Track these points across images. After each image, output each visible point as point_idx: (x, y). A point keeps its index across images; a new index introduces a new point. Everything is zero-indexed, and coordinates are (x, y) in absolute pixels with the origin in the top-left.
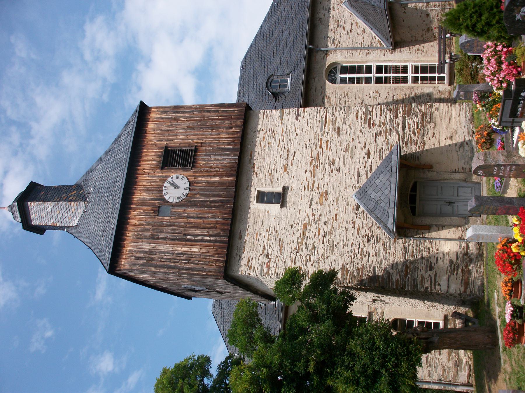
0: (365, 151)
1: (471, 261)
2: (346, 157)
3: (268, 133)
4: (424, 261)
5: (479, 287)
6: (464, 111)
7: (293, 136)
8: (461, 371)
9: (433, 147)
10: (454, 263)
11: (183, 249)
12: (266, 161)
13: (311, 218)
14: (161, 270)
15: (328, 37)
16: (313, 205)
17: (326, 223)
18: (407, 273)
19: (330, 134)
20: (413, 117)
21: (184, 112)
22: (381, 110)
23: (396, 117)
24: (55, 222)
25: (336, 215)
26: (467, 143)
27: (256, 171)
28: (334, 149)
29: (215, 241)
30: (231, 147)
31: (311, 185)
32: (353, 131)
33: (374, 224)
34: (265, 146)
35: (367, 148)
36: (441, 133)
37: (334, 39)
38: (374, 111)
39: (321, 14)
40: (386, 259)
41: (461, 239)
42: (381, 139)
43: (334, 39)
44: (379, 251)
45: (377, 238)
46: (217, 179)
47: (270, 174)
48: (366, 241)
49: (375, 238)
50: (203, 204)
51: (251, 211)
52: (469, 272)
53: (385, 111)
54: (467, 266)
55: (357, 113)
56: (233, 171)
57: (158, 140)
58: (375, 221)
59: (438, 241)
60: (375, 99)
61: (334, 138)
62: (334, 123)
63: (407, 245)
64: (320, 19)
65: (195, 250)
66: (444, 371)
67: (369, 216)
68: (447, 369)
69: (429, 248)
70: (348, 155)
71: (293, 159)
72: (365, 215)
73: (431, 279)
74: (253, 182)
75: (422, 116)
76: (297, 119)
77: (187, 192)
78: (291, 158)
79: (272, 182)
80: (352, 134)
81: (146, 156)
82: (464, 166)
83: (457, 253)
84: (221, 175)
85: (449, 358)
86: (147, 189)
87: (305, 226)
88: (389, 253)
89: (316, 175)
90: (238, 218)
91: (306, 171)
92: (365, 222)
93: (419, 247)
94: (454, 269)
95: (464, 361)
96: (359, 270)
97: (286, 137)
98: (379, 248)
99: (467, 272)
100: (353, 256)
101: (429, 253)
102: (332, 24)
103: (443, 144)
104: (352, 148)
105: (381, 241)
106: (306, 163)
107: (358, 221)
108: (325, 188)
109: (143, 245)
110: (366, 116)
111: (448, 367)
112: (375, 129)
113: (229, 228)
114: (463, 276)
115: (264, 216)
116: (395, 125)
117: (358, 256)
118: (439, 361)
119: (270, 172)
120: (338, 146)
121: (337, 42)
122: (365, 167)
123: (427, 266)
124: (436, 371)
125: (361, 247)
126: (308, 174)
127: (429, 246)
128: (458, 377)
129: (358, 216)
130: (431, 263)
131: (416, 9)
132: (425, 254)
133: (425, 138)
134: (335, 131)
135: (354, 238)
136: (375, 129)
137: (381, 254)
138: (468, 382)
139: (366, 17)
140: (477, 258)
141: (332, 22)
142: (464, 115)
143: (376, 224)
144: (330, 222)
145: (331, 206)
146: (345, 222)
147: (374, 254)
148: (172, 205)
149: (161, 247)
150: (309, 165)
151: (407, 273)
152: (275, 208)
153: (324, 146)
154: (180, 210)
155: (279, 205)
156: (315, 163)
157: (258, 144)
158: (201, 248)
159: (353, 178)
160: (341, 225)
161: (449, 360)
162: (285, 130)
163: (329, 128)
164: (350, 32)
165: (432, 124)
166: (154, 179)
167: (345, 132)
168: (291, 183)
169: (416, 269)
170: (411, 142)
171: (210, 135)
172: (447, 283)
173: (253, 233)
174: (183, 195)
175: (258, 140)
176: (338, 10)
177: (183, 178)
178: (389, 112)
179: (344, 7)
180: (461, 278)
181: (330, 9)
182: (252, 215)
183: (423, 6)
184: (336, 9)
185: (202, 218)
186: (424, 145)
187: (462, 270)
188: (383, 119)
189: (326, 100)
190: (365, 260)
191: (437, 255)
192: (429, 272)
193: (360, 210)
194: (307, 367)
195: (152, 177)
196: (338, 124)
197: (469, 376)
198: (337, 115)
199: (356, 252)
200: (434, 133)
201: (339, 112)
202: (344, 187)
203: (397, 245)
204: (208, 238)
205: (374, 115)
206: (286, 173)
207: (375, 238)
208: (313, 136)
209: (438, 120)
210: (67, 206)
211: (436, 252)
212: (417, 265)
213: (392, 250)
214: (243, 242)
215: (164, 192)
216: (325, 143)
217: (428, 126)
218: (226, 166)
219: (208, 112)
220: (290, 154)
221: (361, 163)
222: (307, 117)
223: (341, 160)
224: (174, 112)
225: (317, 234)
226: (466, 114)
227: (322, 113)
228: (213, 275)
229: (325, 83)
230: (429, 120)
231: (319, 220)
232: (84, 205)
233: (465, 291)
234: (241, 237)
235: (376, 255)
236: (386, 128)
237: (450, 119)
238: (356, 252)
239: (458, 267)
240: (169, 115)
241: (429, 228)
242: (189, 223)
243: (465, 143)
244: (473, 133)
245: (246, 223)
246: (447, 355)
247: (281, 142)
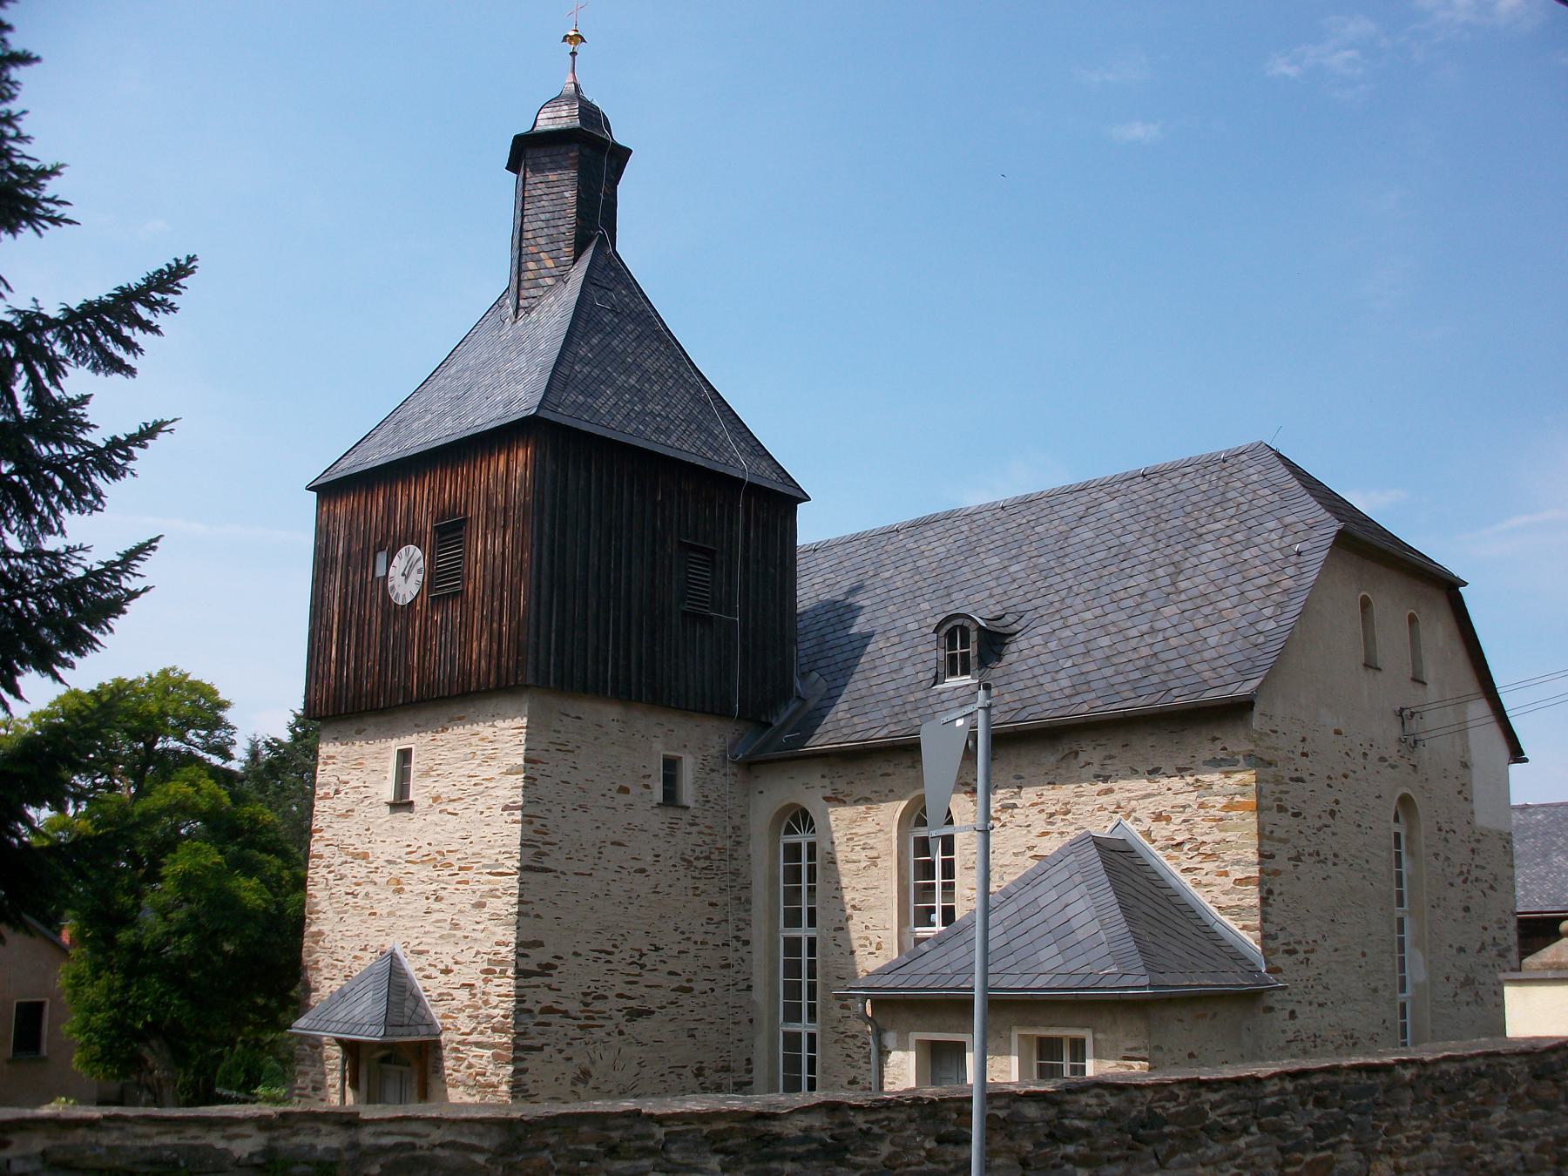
3: (490, 746)
15: (1020, 787)
23: (494, 1030)
37: (1014, 806)
39: (1091, 753)
42: (463, 995)
43: (1014, 806)
60: (863, 942)
62: (492, 893)
64: (1077, 753)
75: (493, 1086)
87: (365, 856)
96: (317, 962)
97: (480, 788)
108: (407, 888)
112: (479, 984)
116: (481, 1028)
121: (1004, 817)
136: (479, 984)
141: (1066, 792)
152: (388, 793)
153: (463, 875)
156: (438, 860)
164: (1032, 853)
170: (458, 1059)
181: (1106, 780)
184: (1104, 799)
189: (862, 808)
208: (476, 849)
227: (509, 863)
229: (901, 799)
234: (359, 732)
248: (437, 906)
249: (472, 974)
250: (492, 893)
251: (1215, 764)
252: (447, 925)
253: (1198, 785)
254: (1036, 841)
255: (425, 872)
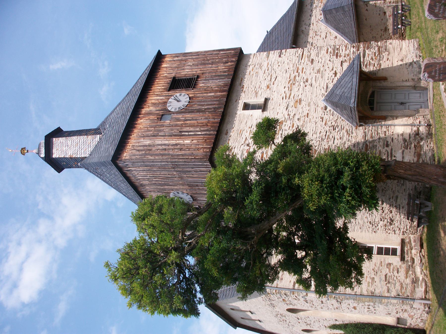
0: (333, 72)
1: (422, 139)
2: (317, 77)
3: (256, 66)
4: (381, 140)
5: (430, 157)
6: (412, 43)
7: (276, 67)
8: (418, 287)
9: (387, 67)
10: (408, 141)
11: (178, 142)
12: (253, 83)
13: (287, 117)
14: (156, 158)
16: (289, 108)
17: (298, 119)
18: (367, 150)
19: (305, 63)
20: (371, 50)
21: (191, 56)
22: (346, 47)
24: (72, 154)
25: (308, 114)
26: (415, 63)
27: (244, 90)
28: (308, 72)
29: (206, 134)
30: (226, 74)
31: (288, 96)
32: (323, 60)
33: (339, 118)
34: (253, 74)
35: (334, 70)
36: (394, 58)
37: (312, 43)
38: (340, 48)
39: (303, 28)
40: (349, 141)
41: (412, 125)
43: (312, 43)
44: (343, 136)
45: (341, 127)
46: (213, 94)
47: (255, 91)
48: (332, 129)
49: (340, 127)
50: (199, 111)
51: (237, 116)
52: (421, 147)
53: (350, 47)
54: (419, 143)
55: (328, 50)
56: (227, 88)
57: (168, 74)
58: (340, 116)
59: (393, 127)
61: (308, 66)
62: (309, 57)
63: (367, 130)
65: (187, 142)
66: (402, 287)
67: (335, 113)
68: (404, 286)
69: (385, 132)
70: (319, 75)
71: (275, 80)
72: (331, 112)
73: (388, 153)
74: (241, 97)
75: (379, 48)
76: (280, 56)
77: (187, 103)
78: (273, 80)
79: (256, 96)
80: (323, 63)
81: (158, 84)
82: (413, 78)
83: (410, 134)
84: (216, 91)
85: (407, 276)
86: (154, 104)
88: (352, 136)
89: (293, 89)
90: (227, 120)
91: (285, 87)
92: (331, 117)
93: (377, 131)
94: (408, 145)
95: (421, 278)
97: (270, 67)
98: (343, 134)
99: (418, 147)
100: (321, 141)
101: (385, 135)
102: (311, 33)
103: (395, 64)
104: (322, 71)
105: (345, 129)
106: (285, 83)
107: (325, 117)
108: (300, 97)
109: (144, 141)
110: (334, 51)
111: (405, 284)
113: (218, 125)
114: (415, 150)
115: (248, 118)
117: (325, 140)
118: (397, 278)
119: (256, 90)
120: (311, 70)
122: (332, 82)
123: (384, 144)
124: (395, 288)
125: (327, 134)
126: (287, 89)
127: (385, 130)
128: (415, 292)
129: (326, 113)
130: (387, 142)
131: (376, 6)
132: (382, 136)
133: (381, 62)
134: (309, 61)
135: (322, 128)
136: (341, 59)
137: (345, 138)
138: (425, 297)
139: (337, 29)
140: (427, 137)
142: (412, 46)
143: (341, 118)
144: (302, 119)
145: (303, 109)
146: (315, 118)
147: (339, 138)
148: (173, 113)
149: (159, 141)
150: (288, 82)
151: (367, 150)
153: (300, 71)
154: (180, 116)
155: (261, 110)
156: (292, 82)
157: (247, 73)
158: (192, 140)
159: (322, 89)
160: (312, 120)
161: (406, 277)
162: (270, 63)
163: (305, 59)
165: (387, 53)
166: (161, 98)
167: (318, 61)
168: (272, 96)
169: (375, 147)
170: (370, 65)
171: (211, 68)
172: (402, 155)
173: (238, 130)
174: (183, 106)
175: (248, 71)
176: (317, 25)
177: (184, 95)
178: (352, 48)
179: (321, 23)
180: (414, 151)
181: (310, 24)
182: (238, 118)
183: (381, 3)
184: (314, 25)
185: (196, 120)
186: (380, 66)
187: (415, 146)
188: (348, 52)
190: (331, 143)
191: (392, 137)
192: (386, 148)
193: (328, 110)
194: (277, 168)
195: (160, 96)
196: (312, 57)
197: (426, 292)
198: (311, 52)
199: (324, 137)
200: (388, 58)
201: (313, 50)
202: (315, 95)
203: (358, 131)
204: (200, 133)
205: (341, 50)
206: (268, 89)
207: (340, 127)
208: (291, 65)
209: (391, 50)
210: (85, 140)
211: (391, 134)
212: (375, 144)
213: (354, 134)
214: (228, 137)
215: (168, 105)
216: (301, 69)
217: (384, 54)
218: (220, 86)
219: (210, 54)
220: (272, 78)
221: (329, 80)
222: (287, 54)
223: (314, 79)
224: (184, 56)
225: (291, 128)
226: (414, 45)
228: (200, 158)
230: (384, 51)
231: (294, 117)
232: (99, 138)
233: (418, 160)
234: (227, 133)
235: (340, 139)
236: (350, 57)
237: (401, 49)
238: (324, 137)
239: (411, 143)
240: (180, 58)
241: (385, 118)
242: (185, 124)
243: (413, 63)
244: (420, 56)
245: (232, 123)
246: (405, 273)
247: (266, 71)
248: (309, 81)
249: (337, 62)
250: (309, 57)
251: (312, 5)
252: (318, 75)
253: (316, 8)
254: (322, 38)
255: (295, 88)
